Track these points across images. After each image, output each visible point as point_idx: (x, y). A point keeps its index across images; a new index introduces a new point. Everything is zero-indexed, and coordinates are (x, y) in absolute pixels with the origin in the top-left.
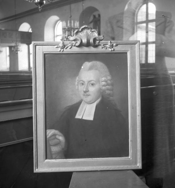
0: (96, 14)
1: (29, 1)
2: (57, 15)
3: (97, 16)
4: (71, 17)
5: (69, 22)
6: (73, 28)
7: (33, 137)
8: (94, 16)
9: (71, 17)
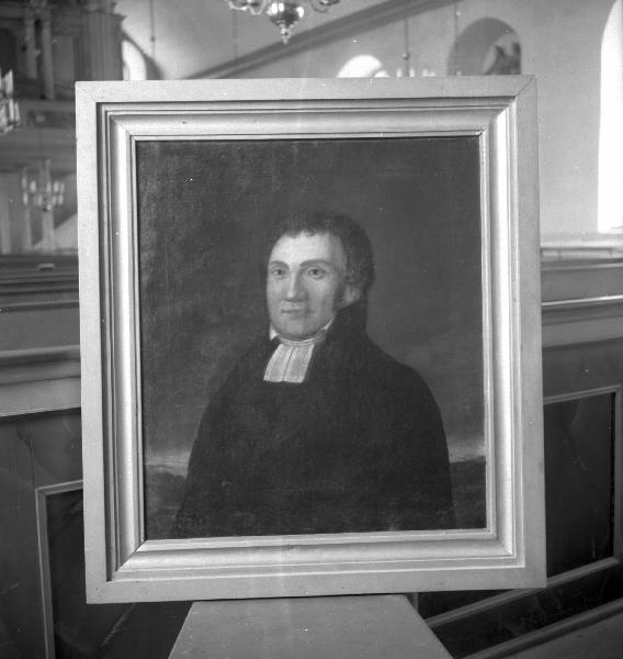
0: (505, 43)
3: (509, 52)
4: (407, 58)
8: (501, 52)
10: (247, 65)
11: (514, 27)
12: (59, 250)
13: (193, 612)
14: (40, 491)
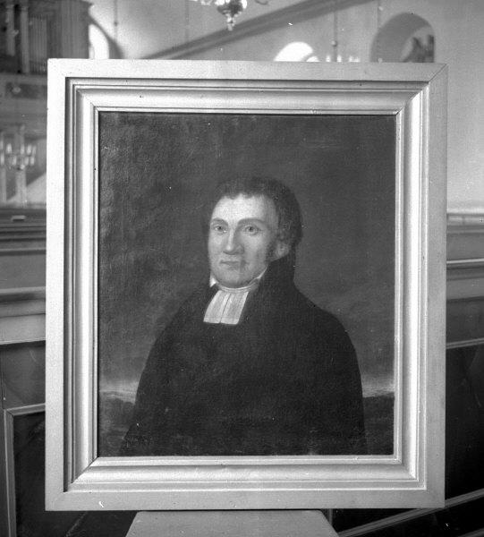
0: (422, 35)
1: (203, 3)
2: (306, 42)
3: (425, 42)
4: (335, 46)
8: (417, 43)
9: (335, 46)
11: (430, 22)
13: (137, 520)
14: (8, 413)
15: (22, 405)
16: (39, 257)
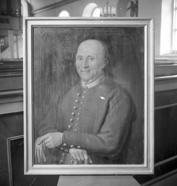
3: (135, 3)
4: (107, 3)
5: (105, 8)
6: (109, 14)
7: (23, 134)
8: (132, 3)
9: (107, 3)
10: (61, 4)
12: (2, 59)
13: (60, 180)
14: (8, 139)
15: (14, 136)
16: (19, 78)
